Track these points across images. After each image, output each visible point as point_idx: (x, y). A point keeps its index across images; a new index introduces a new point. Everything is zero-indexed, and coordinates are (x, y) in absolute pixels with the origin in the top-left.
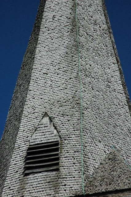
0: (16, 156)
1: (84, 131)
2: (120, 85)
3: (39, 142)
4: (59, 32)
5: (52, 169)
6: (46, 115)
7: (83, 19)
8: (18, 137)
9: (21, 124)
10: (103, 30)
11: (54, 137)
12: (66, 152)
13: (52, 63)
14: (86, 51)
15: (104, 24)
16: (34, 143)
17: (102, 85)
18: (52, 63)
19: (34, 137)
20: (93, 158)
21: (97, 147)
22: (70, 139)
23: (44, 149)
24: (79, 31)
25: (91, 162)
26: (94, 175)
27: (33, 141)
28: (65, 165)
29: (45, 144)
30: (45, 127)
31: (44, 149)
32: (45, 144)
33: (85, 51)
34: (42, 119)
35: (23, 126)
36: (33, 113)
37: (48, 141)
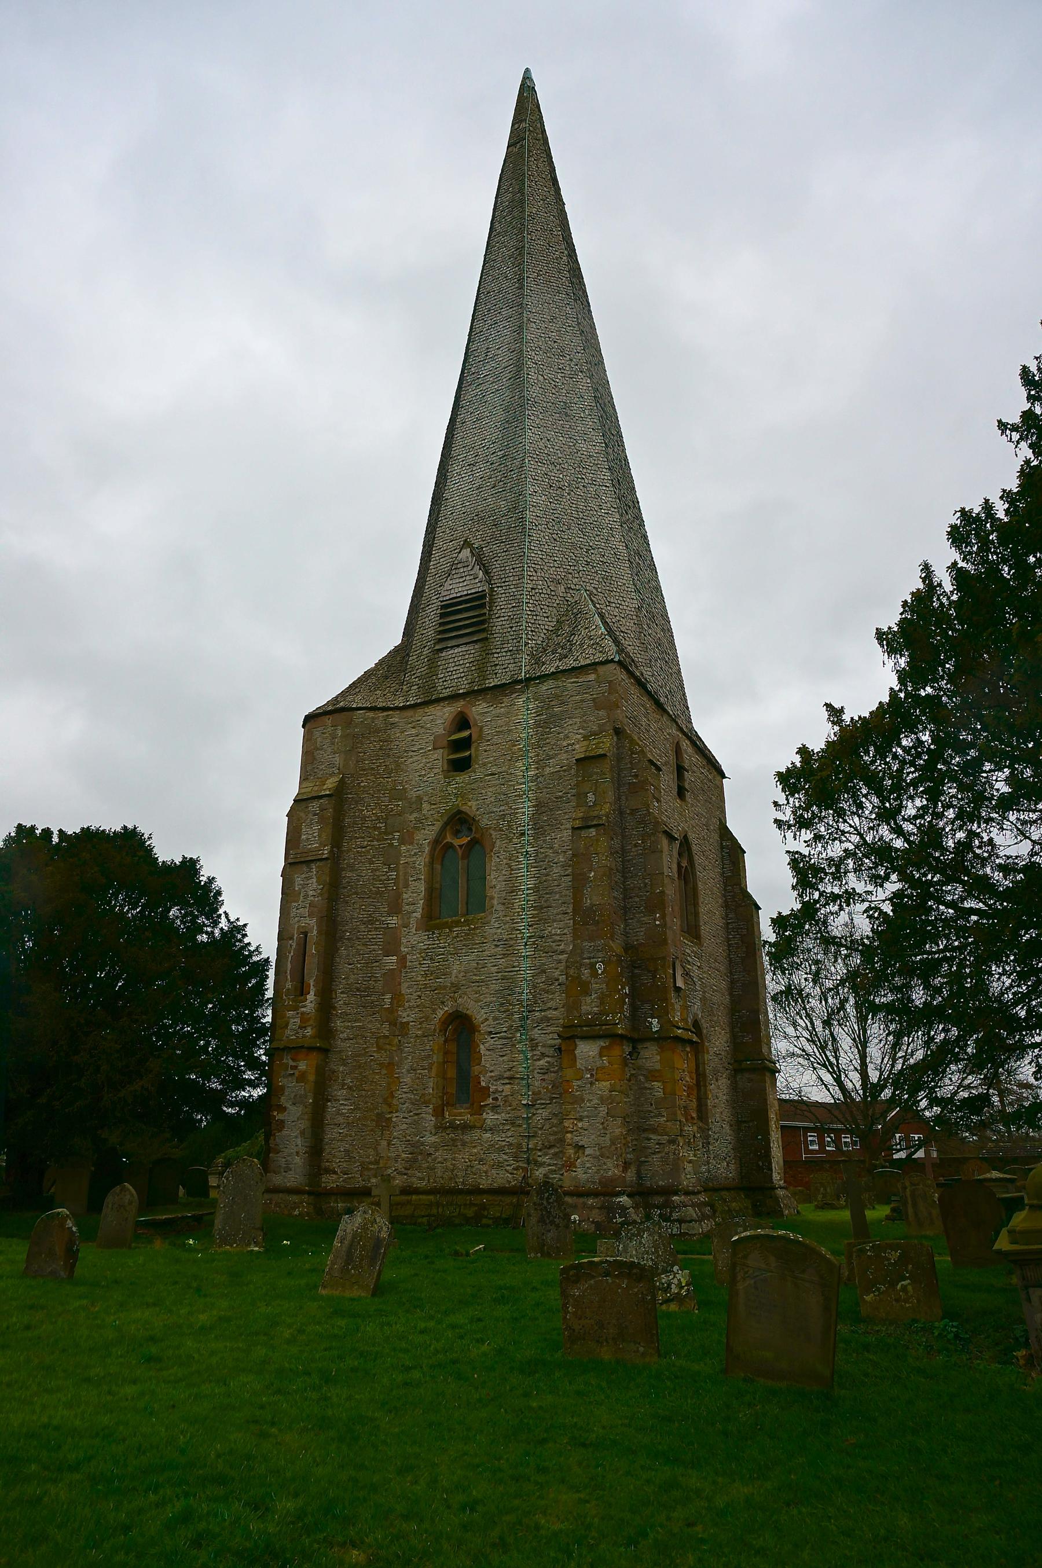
0: (423, 620)
1: (529, 567)
2: (604, 470)
3: (455, 595)
4: (495, 380)
5: (447, 636)
6: (467, 544)
7: (538, 349)
8: (427, 587)
9: (432, 563)
10: (577, 365)
11: (479, 585)
12: (498, 608)
13: (482, 444)
14: (541, 413)
15: (578, 353)
16: (448, 598)
17: (569, 475)
18: (482, 444)
19: (447, 586)
20: (545, 615)
21: (553, 593)
22: (507, 584)
23: (453, 609)
24: (528, 374)
25: (540, 622)
26: (545, 644)
27: (446, 593)
28: (497, 631)
29: (475, 595)
30: (464, 567)
31: (453, 609)
32: (475, 595)
33: (539, 413)
34: (460, 552)
35: (435, 566)
36: (450, 542)
37: (469, 592)
